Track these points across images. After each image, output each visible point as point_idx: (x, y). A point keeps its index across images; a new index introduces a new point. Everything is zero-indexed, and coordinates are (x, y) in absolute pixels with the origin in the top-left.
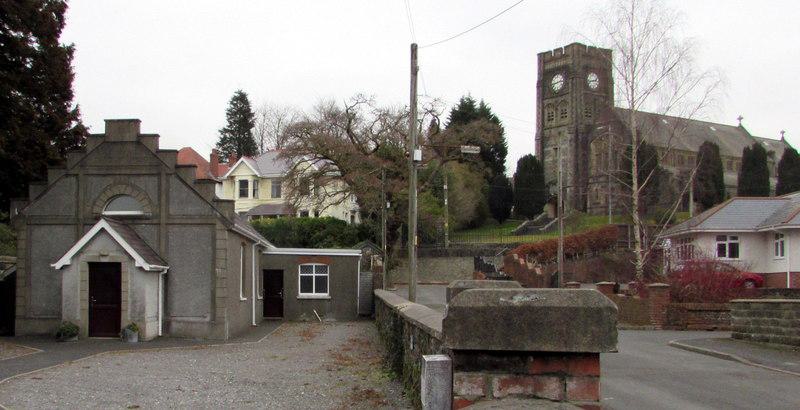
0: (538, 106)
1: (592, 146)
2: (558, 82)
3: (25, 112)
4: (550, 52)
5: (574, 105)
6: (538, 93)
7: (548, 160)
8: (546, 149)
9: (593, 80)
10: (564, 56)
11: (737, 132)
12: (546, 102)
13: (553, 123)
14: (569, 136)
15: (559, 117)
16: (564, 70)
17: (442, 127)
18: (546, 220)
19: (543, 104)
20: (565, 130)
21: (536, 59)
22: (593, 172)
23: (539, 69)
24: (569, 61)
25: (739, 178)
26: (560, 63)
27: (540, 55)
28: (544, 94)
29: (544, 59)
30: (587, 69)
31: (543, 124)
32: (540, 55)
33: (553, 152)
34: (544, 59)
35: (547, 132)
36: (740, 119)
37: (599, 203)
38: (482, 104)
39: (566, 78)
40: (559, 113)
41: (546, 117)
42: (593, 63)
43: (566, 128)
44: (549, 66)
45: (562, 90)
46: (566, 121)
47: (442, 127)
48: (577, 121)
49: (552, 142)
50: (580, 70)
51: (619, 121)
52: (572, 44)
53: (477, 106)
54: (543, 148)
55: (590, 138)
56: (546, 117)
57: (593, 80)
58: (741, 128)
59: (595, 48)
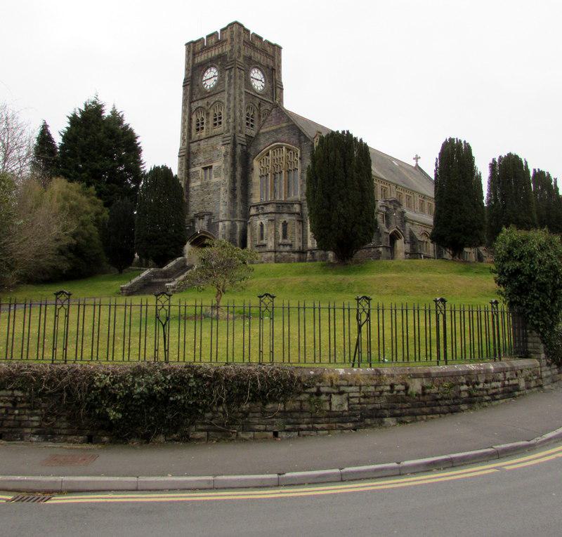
0: (184, 111)
1: (256, 164)
2: (210, 78)
3: (442, 246)
4: (201, 40)
5: (232, 105)
6: (184, 94)
7: (195, 184)
8: (193, 170)
9: (258, 80)
10: (220, 43)
11: (413, 170)
12: (195, 105)
13: (203, 134)
14: (223, 149)
15: (211, 125)
16: (221, 62)
17: (58, 140)
18: (183, 268)
19: (190, 108)
20: (218, 141)
21: (184, 49)
22: (256, 200)
23: (187, 63)
24: (227, 48)
25: (434, 221)
26: (214, 53)
27: (188, 45)
28: (192, 94)
29: (194, 49)
30: (251, 63)
31: (190, 137)
32: (188, 45)
33: (201, 172)
34: (194, 49)
35: (194, 147)
36: (417, 158)
37: (265, 245)
38: (114, 113)
39: (221, 72)
40: (211, 118)
41: (194, 126)
42: (258, 56)
43: (220, 138)
44: (199, 59)
45: (215, 87)
46: (218, 130)
47: (58, 140)
48: (234, 128)
49: (201, 158)
50: (241, 60)
51: (295, 128)
52: (229, 25)
53: (107, 113)
54: (188, 167)
55: (252, 152)
56: (194, 126)
57: (258, 80)
58: (418, 168)
59: (261, 39)
